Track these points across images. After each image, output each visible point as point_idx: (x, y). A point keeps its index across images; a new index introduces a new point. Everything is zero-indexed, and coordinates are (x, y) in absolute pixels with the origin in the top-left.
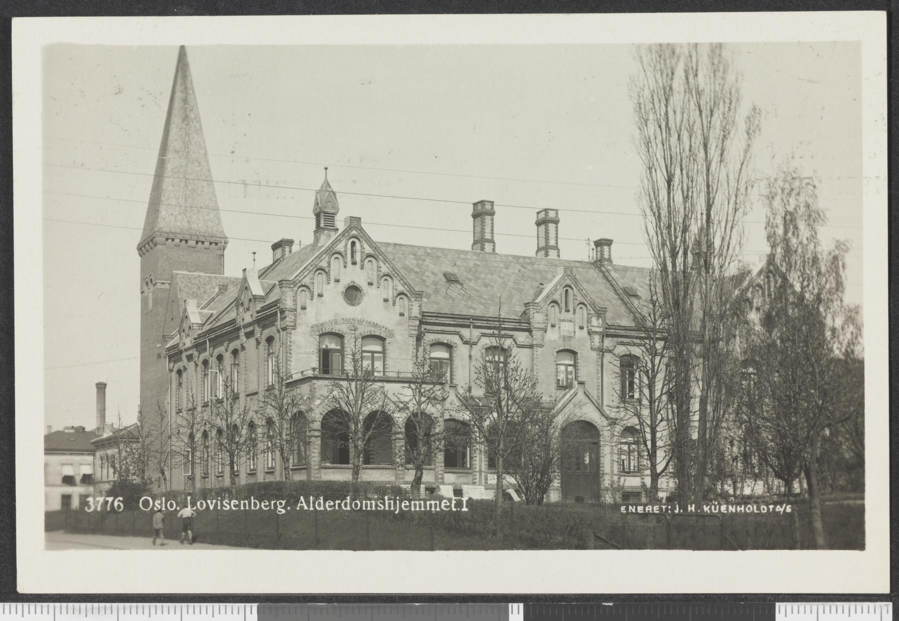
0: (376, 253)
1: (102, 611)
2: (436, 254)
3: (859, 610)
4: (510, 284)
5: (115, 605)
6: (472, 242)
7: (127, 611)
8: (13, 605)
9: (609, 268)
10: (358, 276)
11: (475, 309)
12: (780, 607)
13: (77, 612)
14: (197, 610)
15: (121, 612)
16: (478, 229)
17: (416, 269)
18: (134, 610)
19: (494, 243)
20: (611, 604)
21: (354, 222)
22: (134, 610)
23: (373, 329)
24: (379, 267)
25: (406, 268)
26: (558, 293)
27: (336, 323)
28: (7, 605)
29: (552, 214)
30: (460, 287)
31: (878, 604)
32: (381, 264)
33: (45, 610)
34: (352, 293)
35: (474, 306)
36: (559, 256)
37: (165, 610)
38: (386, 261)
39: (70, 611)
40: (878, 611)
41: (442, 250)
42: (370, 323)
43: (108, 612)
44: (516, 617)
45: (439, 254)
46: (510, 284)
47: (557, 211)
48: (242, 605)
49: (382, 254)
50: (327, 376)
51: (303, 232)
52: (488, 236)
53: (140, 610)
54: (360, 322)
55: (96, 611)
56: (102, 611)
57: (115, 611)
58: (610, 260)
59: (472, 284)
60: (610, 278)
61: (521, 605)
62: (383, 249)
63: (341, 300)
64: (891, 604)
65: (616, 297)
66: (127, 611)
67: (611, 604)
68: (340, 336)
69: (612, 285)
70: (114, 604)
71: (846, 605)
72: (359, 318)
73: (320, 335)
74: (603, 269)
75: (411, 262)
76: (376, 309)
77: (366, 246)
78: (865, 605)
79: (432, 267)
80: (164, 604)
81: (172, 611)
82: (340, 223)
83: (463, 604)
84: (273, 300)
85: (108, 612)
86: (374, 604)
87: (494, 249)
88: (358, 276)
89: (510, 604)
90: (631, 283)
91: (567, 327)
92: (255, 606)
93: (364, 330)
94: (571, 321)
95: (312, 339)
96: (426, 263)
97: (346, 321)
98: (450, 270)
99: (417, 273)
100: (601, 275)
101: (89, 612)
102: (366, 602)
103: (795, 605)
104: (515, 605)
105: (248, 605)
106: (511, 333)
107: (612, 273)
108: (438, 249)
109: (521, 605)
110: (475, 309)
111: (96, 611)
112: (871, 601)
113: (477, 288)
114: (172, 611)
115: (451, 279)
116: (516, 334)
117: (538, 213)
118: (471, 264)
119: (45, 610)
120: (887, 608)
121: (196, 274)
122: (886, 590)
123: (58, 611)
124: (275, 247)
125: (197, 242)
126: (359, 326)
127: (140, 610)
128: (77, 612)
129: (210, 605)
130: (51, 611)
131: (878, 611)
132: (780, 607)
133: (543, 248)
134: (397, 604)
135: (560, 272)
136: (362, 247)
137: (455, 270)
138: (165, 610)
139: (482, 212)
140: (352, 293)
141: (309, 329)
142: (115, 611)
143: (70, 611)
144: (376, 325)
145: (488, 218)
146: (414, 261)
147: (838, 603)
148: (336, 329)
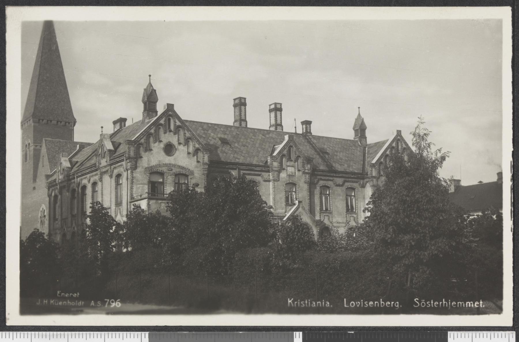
0: (184, 125)
1: (59, 336)
2: (214, 127)
3: (37, 336)
4: (257, 145)
5: (66, 333)
6: (234, 121)
7: (74, 336)
8: (7, 333)
9: (310, 137)
10: (173, 139)
11: (239, 159)
12: (450, 334)
13: (44, 337)
14: (114, 335)
15: (70, 337)
16: (237, 114)
17: (204, 136)
18: (77, 336)
19: (246, 122)
20: (353, 332)
21: (170, 107)
22: (77, 336)
23: (181, 170)
24: (185, 133)
25: (199, 135)
26: (286, 150)
27: (160, 167)
28: (4, 333)
29: (278, 106)
30: (229, 146)
31: (507, 332)
32: (186, 132)
33: (26, 336)
34: (169, 149)
35: (239, 157)
36: (282, 130)
37: (95, 335)
38: (189, 130)
39: (40, 337)
40: (507, 336)
41: (218, 125)
42: (180, 166)
43: (62, 336)
44: (298, 340)
45: (216, 127)
46: (257, 145)
47: (281, 104)
48: (140, 333)
49: (186, 126)
50: (154, 197)
51: (135, 113)
52: (243, 118)
53: (81, 336)
54: (174, 166)
55: (55, 336)
56: (59, 336)
57: (66, 336)
58: (310, 133)
59: (236, 145)
60: (312, 143)
61: (301, 333)
62: (187, 124)
63: (163, 153)
64: (515, 332)
65: (316, 153)
66: (74, 336)
67: (353, 332)
68: (162, 174)
69: (313, 147)
70: (40, 332)
71: (489, 333)
72: (173, 163)
73: (150, 174)
74: (307, 137)
75: (200, 131)
76: (182, 158)
77: (177, 121)
78: (500, 333)
79: (212, 134)
80: (95, 332)
81: (99, 336)
82: (160, 108)
83: (267, 332)
84: (122, 151)
85: (62, 336)
86: (216, 332)
87: (246, 125)
88: (173, 139)
89: (294, 333)
90: (323, 146)
91: (291, 170)
92: (147, 333)
93: (175, 170)
94: (293, 166)
95: (145, 176)
96: (209, 132)
97: (166, 165)
98: (223, 136)
99: (204, 138)
100: (306, 140)
101: (51, 337)
102: (211, 331)
103: (459, 333)
104: (297, 333)
105: (143, 333)
106: (259, 173)
107: (312, 139)
108: (215, 124)
109: (301, 333)
110: (239, 159)
111: (55, 336)
112: (503, 331)
113: (239, 147)
114: (99, 336)
115: (224, 142)
116: (263, 173)
117: (270, 105)
118: (234, 134)
119: (26, 336)
120: (512, 336)
121: (58, 140)
122: (510, 324)
123: (106, 336)
124: (115, 123)
125: (58, 122)
126: (173, 168)
127: (81, 336)
128: (44, 337)
129: (121, 333)
130: (29, 336)
131: (507, 336)
132: (450, 334)
133: (273, 125)
134: (229, 332)
135: (287, 138)
136: (175, 122)
137: (226, 137)
138: (95, 335)
139: (240, 104)
140: (169, 149)
141: (143, 170)
142: (66, 336)
143: (40, 337)
144: (183, 168)
145: (243, 107)
146: (202, 131)
147: (484, 332)
148: (160, 169)
